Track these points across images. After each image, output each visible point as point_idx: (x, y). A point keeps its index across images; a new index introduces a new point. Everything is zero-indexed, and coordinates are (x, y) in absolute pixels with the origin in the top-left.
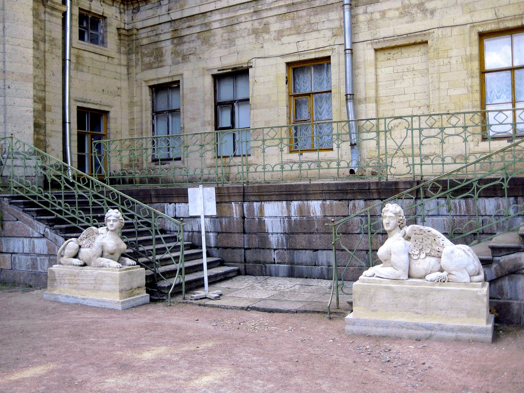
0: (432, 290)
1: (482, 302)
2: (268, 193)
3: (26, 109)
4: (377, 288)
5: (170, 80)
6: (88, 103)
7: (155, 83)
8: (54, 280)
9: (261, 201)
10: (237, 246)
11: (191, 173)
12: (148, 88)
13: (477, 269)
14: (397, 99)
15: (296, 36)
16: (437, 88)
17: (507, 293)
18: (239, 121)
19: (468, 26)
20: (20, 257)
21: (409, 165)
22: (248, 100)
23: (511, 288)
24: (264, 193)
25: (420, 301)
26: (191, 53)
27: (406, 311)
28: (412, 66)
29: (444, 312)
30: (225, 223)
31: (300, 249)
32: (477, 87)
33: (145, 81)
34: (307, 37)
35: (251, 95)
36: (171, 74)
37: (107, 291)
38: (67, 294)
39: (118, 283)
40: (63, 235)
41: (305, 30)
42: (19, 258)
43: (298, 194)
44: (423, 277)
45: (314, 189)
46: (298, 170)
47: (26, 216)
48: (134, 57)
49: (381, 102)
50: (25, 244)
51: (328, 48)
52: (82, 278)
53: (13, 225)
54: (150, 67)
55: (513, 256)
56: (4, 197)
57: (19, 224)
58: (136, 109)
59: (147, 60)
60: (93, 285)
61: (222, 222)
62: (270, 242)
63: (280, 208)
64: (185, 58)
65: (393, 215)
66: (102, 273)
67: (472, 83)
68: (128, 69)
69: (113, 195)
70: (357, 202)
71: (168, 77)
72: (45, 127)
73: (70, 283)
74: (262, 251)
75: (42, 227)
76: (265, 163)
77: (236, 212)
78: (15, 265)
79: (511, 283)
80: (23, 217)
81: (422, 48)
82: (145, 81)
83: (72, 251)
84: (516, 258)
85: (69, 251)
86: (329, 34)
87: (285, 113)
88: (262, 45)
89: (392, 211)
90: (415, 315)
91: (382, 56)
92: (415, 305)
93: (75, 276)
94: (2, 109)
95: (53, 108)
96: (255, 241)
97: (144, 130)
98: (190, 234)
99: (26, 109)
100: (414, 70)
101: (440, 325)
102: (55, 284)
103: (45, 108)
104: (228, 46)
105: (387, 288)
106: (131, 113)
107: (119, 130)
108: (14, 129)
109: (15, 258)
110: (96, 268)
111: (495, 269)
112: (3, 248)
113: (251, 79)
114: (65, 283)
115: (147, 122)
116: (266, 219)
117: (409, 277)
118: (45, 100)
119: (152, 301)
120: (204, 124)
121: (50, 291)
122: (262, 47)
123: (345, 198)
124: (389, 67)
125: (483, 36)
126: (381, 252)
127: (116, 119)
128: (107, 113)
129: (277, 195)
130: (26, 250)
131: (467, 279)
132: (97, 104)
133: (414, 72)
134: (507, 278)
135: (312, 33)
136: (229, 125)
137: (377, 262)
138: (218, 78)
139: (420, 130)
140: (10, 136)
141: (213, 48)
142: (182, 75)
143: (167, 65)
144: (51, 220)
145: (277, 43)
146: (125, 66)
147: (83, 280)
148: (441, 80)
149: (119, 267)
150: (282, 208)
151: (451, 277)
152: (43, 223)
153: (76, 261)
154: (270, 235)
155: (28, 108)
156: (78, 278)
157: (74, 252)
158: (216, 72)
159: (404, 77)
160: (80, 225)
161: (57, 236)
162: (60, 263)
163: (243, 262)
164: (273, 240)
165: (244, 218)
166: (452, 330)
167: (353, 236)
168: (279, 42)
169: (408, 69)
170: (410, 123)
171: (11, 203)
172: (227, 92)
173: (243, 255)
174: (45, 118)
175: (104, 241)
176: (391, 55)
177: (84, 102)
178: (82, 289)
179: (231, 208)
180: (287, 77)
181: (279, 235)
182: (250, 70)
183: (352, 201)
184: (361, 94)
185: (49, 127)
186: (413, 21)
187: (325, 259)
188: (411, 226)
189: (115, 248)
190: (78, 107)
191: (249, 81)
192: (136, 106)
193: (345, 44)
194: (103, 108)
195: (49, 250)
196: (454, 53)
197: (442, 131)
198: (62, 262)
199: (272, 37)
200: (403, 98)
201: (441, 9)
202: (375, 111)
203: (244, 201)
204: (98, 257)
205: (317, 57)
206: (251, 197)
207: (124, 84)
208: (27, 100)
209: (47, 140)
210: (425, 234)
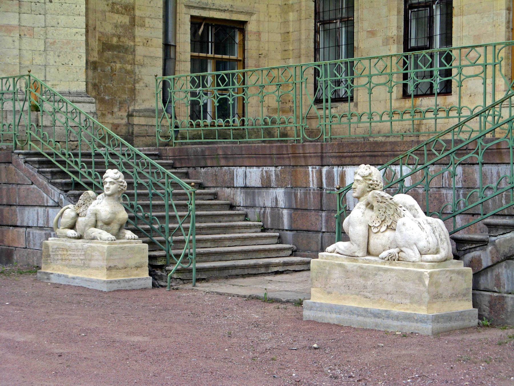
0: (379, 269)
2: (350, 154)
3: (75, 30)
6: (210, 9)
8: (49, 256)
17: (504, 284)
20: (35, 231)
24: (345, 154)
25: (369, 283)
27: (357, 295)
29: (390, 296)
42: (33, 234)
44: (378, 256)
46: (368, 122)
47: (40, 179)
50: (39, 214)
52: (74, 253)
53: (28, 189)
56: (19, 154)
57: (34, 188)
58: (292, 16)
65: (361, 179)
72: (134, 51)
73: (62, 260)
77: (313, 181)
78: (29, 242)
79: (508, 271)
80: (38, 180)
83: (68, 220)
92: (365, 287)
93: (67, 251)
94: (42, 33)
95: (147, 20)
98: (262, 211)
99: (75, 30)
101: (386, 311)
103: (134, 21)
105: (340, 265)
106: (286, 22)
107: (264, 52)
108: (57, 60)
109: (29, 233)
110: (87, 241)
111: (491, 252)
112: (17, 220)
114: (58, 260)
115: (307, 38)
117: (368, 253)
118: (133, 9)
119: (154, 286)
127: (259, 33)
128: (241, 26)
129: (336, 157)
130: (41, 223)
132: (225, 11)
134: (504, 263)
140: (27, 73)
144: (66, 184)
147: (74, 255)
149: (110, 239)
151: (401, 254)
152: (58, 188)
153: (71, 233)
155: (77, 30)
165: (321, 188)
166: (397, 318)
171: (26, 162)
173: (320, 242)
174: (134, 37)
175: (98, 207)
177: (203, 9)
179: (307, 174)
185: (140, 51)
189: (109, 216)
190: (192, 17)
192: (293, 11)
194: (235, 17)
198: (58, 234)
203: (323, 166)
204: (91, 227)
208: (76, 17)
209: (137, 71)
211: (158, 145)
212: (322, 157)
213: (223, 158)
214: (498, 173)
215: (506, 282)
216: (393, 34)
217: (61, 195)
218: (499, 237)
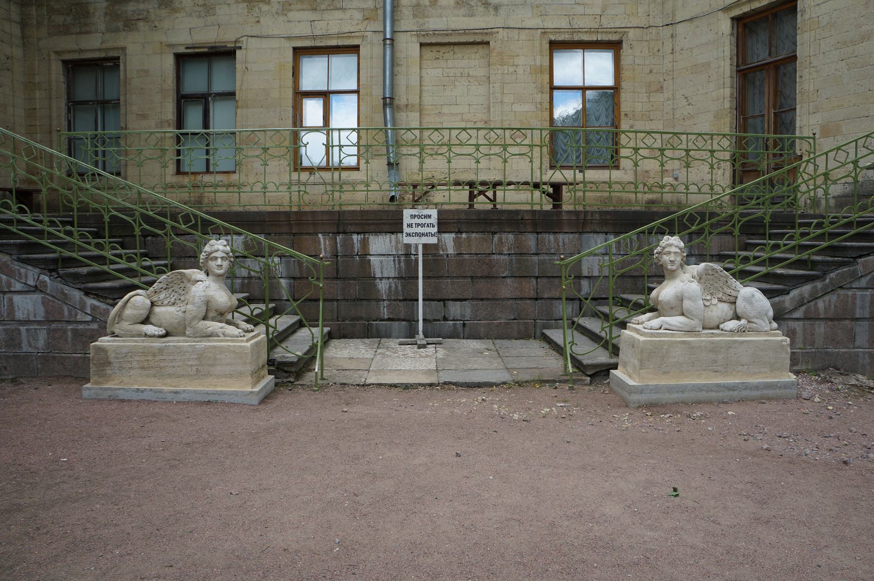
1: (787, 352)
4: (672, 344)
5: (103, 55)
7: (76, 56)
9: (364, 233)
12: (61, 63)
15: (311, 12)
19: (539, 31)
25: (720, 357)
26: (141, 17)
27: (704, 370)
28: (466, 71)
33: (57, 53)
34: (326, 15)
35: (238, 88)
36: (104, 46)
37: (226, 376)
41: (323, 7)
48: (33, 11)
49: (425, 112)
51: (357, 34)
52: (171, 357)
54: (64, 30)
59: (59, 19)
60: (194, 369)
62: (378, 291)
63: (393, 243)
64: (130, 25)
66: (215, 347)
68: (22, 30)
70: (504, 236)
71: (100, 50)
73: (143, 368)
74: (365, 303)
75: (32, 275)
76: (267, 181)
77: (325, 248)
81: (482, 51)
82: (57, 53)
84: (780, 302)
85: (135, 312)
86: (358, 16)
88: (257, 19)
90: (714, 374)
91: (429, 53)
93: (154, 355)
96: (355, 289)
100: (469, 75)
102: (109, 372)
104: (203, 14)
105: (683, 342)
114: (131, 368)
116: (372, 258)
121: (97, 383)
122: (258, 22)
123: (489, 230)
124: (436, 70)
125: (299, 52)
129: (390, 224)
133: (469, 79)
135: (333, 12)
136: (320, 123)
138: (181, 59)
141: (178, 15)
142: (124, 49)
143: (97, 32)
145: (281, 18)
146: (18, 23)
147: (172, 361)
148: (505, 91)
154: (378, 280)
156: (161, 357)
157: (144, 313)
158: (182, 50)
160: (112, 267)
161: (67, 287)
162: (113, 334)
164: (383, 286)
167: (498, 280)
168: (285, 18)
172: (195, 82)
176: (441, 53)
178: (170, 376)
181: (391, 280)
182: (238, 52)
184: (401, 100)
186: (472, 16)
187: (459, 311)
193: (384, 32)
195: (47, 312)
196: (520, 61)
198: (117, 331)
199: (274, 10)
200: (455, 110)
201: (508, 5)
203: (339, 233)
205: (340, 44)
207: (18, 52)
211: (61, 209)
212: (338, 225)
214: (563, 239)
217: (42, 277)
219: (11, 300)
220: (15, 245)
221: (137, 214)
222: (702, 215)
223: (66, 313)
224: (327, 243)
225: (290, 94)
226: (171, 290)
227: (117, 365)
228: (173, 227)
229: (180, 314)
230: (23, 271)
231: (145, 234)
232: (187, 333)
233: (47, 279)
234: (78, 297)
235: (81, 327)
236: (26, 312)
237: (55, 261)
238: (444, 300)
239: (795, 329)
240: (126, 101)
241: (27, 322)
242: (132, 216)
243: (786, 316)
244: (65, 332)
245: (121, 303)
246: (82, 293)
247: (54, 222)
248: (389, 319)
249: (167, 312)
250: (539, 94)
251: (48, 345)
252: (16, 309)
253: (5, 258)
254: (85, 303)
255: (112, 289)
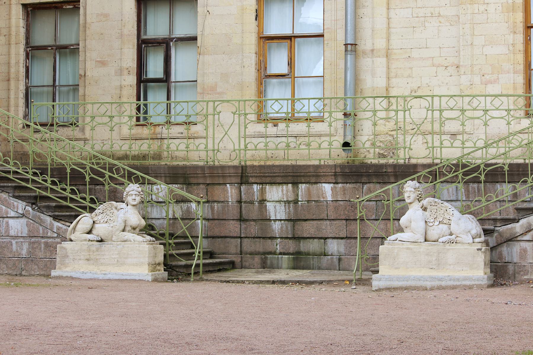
9: (262, 184)
10: (231, 235)
11: (97, 147)
12: (21, 7)
13: (479, 233)
14: (415, 54)
16: (469, 43)
18: (175, 70)
21: (428, 148)
22: (195, 39)
23: (508, 253)
24: (267, 174)
27: (423, 267)
29: (452, 266)
30: (218, 208)
31: (308, 238)
32: (520, 46)
38: (82, 270)
39: (147, 256)
40: (50, 214)
43: (307, 176)
45: (325, 170)
55: (509, 226)
60: (116, 260)
61: (214, 207)
62: (273, 231)
63: (285, 192)
65: (413, 190)
67: (514, 40)
69: (118, 170)
75: (21, 206)
77: (231, 196)
84: (512, 228)
87: (254, 63)
89: (410, 188)
96: (254, 229)
97: (12, 76)
101: (449, 276)
102: (67, 261)
105: (408, 249)
111: (496, 237)
113: (200, 9)
115: (17, 63)
120: (120, 72)
126: (403, 220)
129: (282, 176)
131: (471, 240)
133: (440, 19)
134: (505, 244)
136: (160, 74)
137: (401, 230)
139: (441, 111)
150: (287, 191)
156: (97, 253)
157: (89, 227)
159: (427, 24)
161: (42, 215)
163: (239, 253)
169: (432, 14)
170: (431, 104)
180: (257, 10)
183: (368, 185)
184: (365, 44)
187: (336, 248)
188: (427, 199)
191: (196, 12)
195: (29, 231)
197: (463, 114)
202: (385, 69)
206: (251, 179)
210: (439, 206)
213: (210, 176)
215: (506, 255)
216: (128, 65)
217: (27, 207)
218: (502, 227)
219: (7, 223)
220: (11, 187)
221: (88, 168)
222: (457, 165)
223: (41, 232)
224: (233, 191)
225: (252, 40)
226: (105, 214)
227: (72, 257)
228: (110, 177)
229: (110, 229)
230: (15, 203)
231: (93, 182)
232: (113, 239)
233: (30, 209)
234: (49, 221)
235: (50, 240)
236: (16, 231)
237: (36, 198)
238: (325, 239)
239: (526, 248)
240: (85, 47)
241: (17, 237)
242: (84, 168)
243: (519, 239)
244: (40, 243)
245: (75, 222)
246: (52, 218)
247: (37, 173)
248: (280, 254)
249: (101, 229)
250: (512, 35)
251: (29, 252)
252: (10, 229)
253: (4, 195)
254: (53, 225)
255: (70, 216)
